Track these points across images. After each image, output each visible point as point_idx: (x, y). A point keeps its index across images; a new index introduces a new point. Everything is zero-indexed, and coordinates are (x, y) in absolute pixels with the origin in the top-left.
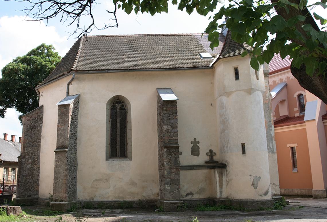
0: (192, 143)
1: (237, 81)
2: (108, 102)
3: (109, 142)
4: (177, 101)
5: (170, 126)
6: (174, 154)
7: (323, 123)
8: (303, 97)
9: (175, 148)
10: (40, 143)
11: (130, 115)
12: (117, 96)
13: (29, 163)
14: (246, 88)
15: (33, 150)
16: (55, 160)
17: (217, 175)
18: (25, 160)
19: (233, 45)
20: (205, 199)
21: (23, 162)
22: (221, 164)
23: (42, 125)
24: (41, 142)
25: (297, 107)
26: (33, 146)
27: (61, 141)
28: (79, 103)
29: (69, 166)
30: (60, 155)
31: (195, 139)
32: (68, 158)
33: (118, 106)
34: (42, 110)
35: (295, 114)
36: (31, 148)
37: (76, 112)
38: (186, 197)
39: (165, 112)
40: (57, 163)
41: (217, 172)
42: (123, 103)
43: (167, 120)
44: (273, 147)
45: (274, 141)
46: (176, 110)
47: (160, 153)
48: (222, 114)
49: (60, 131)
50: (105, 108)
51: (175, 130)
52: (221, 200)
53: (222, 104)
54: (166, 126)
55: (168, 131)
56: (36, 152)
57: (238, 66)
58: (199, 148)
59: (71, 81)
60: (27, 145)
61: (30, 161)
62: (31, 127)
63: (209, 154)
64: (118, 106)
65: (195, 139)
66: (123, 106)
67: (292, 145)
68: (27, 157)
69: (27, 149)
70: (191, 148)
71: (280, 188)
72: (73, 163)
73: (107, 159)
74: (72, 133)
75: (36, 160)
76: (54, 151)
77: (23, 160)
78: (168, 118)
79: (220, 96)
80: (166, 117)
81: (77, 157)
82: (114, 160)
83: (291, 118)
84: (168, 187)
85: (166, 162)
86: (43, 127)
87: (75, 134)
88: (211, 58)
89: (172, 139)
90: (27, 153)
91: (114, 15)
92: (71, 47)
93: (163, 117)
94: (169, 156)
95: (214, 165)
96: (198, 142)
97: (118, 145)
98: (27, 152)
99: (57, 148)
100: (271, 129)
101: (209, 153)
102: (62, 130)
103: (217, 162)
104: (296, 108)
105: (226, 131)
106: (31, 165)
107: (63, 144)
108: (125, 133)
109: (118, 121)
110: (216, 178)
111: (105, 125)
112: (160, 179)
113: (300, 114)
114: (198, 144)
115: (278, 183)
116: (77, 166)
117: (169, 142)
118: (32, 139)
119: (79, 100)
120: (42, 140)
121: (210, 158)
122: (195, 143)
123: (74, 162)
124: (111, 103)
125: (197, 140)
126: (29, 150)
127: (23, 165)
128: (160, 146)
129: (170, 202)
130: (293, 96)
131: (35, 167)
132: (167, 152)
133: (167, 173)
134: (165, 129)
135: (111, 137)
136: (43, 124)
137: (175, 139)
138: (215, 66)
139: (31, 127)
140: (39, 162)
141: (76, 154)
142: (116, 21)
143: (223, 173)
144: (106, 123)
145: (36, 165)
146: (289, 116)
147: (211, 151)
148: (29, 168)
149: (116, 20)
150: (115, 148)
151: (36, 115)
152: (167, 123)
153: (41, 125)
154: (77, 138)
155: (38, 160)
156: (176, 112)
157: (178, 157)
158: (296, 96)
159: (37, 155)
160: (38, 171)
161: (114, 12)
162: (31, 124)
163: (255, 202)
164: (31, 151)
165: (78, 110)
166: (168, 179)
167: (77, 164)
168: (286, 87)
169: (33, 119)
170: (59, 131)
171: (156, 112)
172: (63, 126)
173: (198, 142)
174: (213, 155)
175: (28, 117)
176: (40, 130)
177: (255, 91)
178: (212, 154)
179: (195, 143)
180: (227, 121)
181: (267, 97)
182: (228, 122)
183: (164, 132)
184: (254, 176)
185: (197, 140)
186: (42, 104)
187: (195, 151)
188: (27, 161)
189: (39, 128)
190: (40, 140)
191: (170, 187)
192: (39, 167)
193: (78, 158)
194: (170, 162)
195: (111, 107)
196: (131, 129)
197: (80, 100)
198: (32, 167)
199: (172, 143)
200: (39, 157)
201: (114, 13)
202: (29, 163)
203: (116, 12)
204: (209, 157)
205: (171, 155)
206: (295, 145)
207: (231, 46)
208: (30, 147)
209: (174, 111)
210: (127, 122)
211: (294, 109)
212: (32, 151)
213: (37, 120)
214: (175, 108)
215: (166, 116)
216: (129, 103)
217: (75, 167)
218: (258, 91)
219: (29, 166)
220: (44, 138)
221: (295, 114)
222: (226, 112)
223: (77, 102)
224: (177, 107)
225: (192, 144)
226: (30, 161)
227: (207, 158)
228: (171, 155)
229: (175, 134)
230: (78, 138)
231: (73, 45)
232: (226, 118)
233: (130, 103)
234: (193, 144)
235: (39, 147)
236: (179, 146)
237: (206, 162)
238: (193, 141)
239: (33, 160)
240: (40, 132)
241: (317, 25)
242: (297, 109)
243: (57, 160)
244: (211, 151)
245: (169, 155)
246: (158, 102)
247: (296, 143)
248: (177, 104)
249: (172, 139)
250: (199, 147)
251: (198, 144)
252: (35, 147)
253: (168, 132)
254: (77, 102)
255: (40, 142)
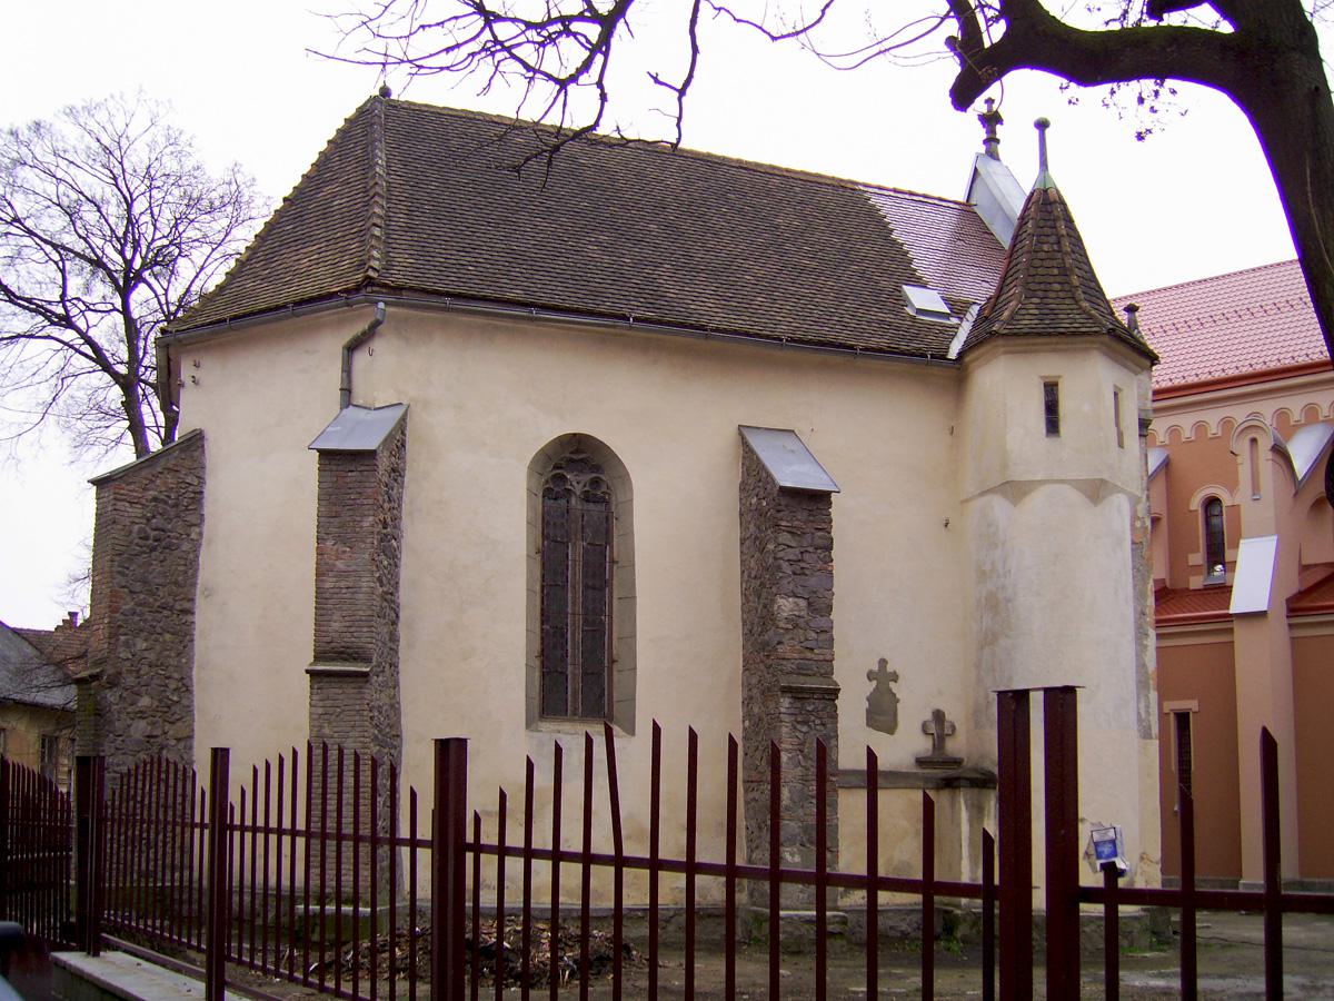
0: (871, 676)
1: (1053, 441)
2: (535, 461)
3: (537, 645)
4: (833, 494)
5: (803, 603)
6: (818, 722)
7: (1287, 627)
8: (1221, 511)
9: (824, 699)
10: (189, 618)
11: (629, 534)
12: (575, 435)
13: (141, 715)
14: (1085, 477)
15: (158, 648)
16: (311, 713)
17: (964, 815)
18: (120, 696)
19: (1042, 286)
20: (911, 905)
21: (111, 704)
22: (975, 770)
23: (201, 534)
24: (197, 611)
25: (1198, 551)
26: (159, 630)
27: (336, 626)
28: (403, 446)
29: (375, 746)
30: (334, 690)
31: (883, 662)
32: (373, 706)
33: (577, 482)
34: (196, 454)
35: (1191, 579)
36: (146, 640)
37: (395, 491)
38: (845, 899)
39: (785, 538)
40: (321, 727)
41: (962, 801)
42: (597, 471)
43: (794, 573)
44: (1148, 713)
45: (1152, 691)
46: (830, 533)
47: (756, 710)
48: (987, 567)
49: (331, 574)
50: (524, 485)
51: (821, 622)
52: (974, 913)
53: (990, 525)
54: (790, 599)
55: (795, 623)
56: (173, 662)
57: (1060, 377)
58: (898, 701)
59: (364, 333)
60: (126, 621)
61: (145, 701)
62: (146, 538)
63: (932, 729)
64: (577, 482)
65: (883, 662)
66: (596, 483)
67: (1181, 705)
68: (130, 680)
69: (126, 644)
70: (868, 700)
71: (1163, 871)
72: (388, 730)
73: (528, 725)
74: (385, 589)
75: (175, 698)
76: (307, 671)
77: (108, 694)
78: (797, 568)
79: (984, 493)
80: (789, 560)
81: (398, 703)
82: (561, 728)
83: (1174, 591)
84: (792, 855)
85: (787, 750)
86: (204, 542)
87: (391, 594)
88: (947, 316)
89: (809, 655)
90: (128, 664)
91: (680, 99)
92: (323, 146)
93: (776, 559)
94: (798, 726)
95: (950, 773)
96: (895, 677)
97: (577, 659)
98: (128, 659)
99: (319, 657)
100: (1145, 642)
101: (933, 726)
102: (342, 575)
103: (957, 762)
104: (1194, 555)
105: (1002, 642)
106: (154, 724)
107: (348, 639)
108: (602, 612)
109: (576, 552)
110: (959, 825)
111: (523, 568)
112: (753, 822)
113: (1205, 580)
114: (892, 685)
115: (1157, 855)
116: (400, 746)
117: (801, 671)
118: (151, 593)
119: (403, 433)
120: (200, 602)
121: (934, 745)
122: (883, 677)
123: (391, 727)
124: (545, 467)
125: (890, 668)
126: (138, 647)
127: (111, 722)
128: (754, 681)
129: (800, 917)
130: (1188, 505)
131: (171, 732)
132: (792, 711)
133: (791, 799)
134: (785, 614)
135: (542, 624)
136: (206, 528)
137: (821, 657)
138: (973, 361)
139: (146, 538)
140: (189, 709)
141: (395, 688)
142: (678, 125)
143: (984, 809)
144: (528, 556)
145: (175, 727)
146: (1168, 585)
147: (939, 716)
148: (138, 736)
149: (679, 119)
150: (561, 673)
151: (171, 479)
152: (791, 587)
153: (197, 530)
154: (397, 616)
155: (184, 702)
156: (827, 543)
157: (832, 734)
158: (1196, 503)
159: (176, 675)
160: (185, 757)
161: (679, 87)
162: (148, 520)
163: (1092, 922)
164: (146, 654)
165: (403, 483)
166: (793, 824)
167: (398, 736)
168: (1164, 471)
169: (155, 499)
170: (324, 575)
171: (736, 534)
172: (344, 552)
173: (895, 677)
174: (946, 732)
175: (131, 483)
176: (191, 556)
177: (1111, 494)
178: (943, 730)
179: (883, 677)
180: (1009, 601)
181: (1139, 518)
182: (1010, 605)
183: (781, 624)
184: (1092, 824)
185: (890, 668)
186: (197, 425)
187: (882, 713)
188: (129, 701)
189: (186, 546)
190: (192, 600)
191: (802, 857)
192: (191, 737)
193: (405, 707)
194: (802, 751)
195: (547, 482)
196: (635, 597)
197: (407, 432)
198: (155, 733)
199: (809, 672)
200: (185, 687)
201: (682, 92)
202: (141, 715)
203: (689, 90)
204: (930, 739)
205: (809, 726)
206: (1191, 705)
207: (1032, 286)
208: (143, 635)
209: (820, 537)
210: (613, 562)
211: (1187, 558)
212: (152, 656)
213: (175, 506)
214: (824, 526)
215: (792, 557)
216: (625, 477)
217: (393, 751)
218: (1119, 492)
219: (140, 728)
220: (209, 593)
221: (1191, 579)
222: (1005, 562)
223: (399, 444)
224: (831, 521)
225: (870, 680)
226: (145, 701)
227: (923, 745)
228: (809, 726)
229: (823, 636)
230: (401, 615)
231: (332, 135)
232: (1003, 587)
233: (628, 474)
234: (875, 683)
235: (183, 636)
236: (835, 692)
237: (920, 762)
238: (876, 668)
239: (160, 701)
240: (191, 566)
241: (1032, 69)
242: (1198, 558)
243: (320, 711)
244: (939, 716)
245: (798, 722)
246: (743, 488)
247: (1193, 698)
248: (833, 510)
249: (809, 655)
250: (898, 696)
251: (892, 685)
252: (168, 637)
253: (796, 626)
254: (399, 444)
255: (191, 612)
